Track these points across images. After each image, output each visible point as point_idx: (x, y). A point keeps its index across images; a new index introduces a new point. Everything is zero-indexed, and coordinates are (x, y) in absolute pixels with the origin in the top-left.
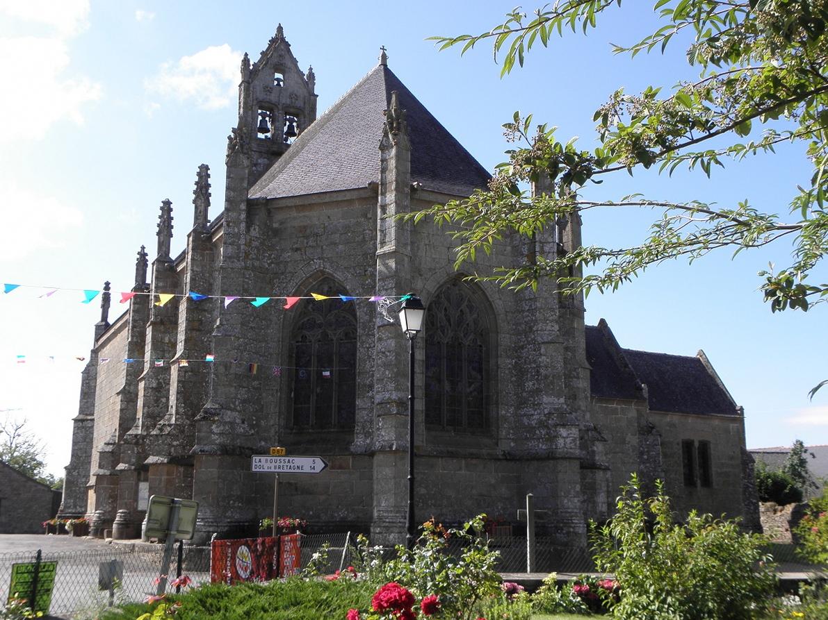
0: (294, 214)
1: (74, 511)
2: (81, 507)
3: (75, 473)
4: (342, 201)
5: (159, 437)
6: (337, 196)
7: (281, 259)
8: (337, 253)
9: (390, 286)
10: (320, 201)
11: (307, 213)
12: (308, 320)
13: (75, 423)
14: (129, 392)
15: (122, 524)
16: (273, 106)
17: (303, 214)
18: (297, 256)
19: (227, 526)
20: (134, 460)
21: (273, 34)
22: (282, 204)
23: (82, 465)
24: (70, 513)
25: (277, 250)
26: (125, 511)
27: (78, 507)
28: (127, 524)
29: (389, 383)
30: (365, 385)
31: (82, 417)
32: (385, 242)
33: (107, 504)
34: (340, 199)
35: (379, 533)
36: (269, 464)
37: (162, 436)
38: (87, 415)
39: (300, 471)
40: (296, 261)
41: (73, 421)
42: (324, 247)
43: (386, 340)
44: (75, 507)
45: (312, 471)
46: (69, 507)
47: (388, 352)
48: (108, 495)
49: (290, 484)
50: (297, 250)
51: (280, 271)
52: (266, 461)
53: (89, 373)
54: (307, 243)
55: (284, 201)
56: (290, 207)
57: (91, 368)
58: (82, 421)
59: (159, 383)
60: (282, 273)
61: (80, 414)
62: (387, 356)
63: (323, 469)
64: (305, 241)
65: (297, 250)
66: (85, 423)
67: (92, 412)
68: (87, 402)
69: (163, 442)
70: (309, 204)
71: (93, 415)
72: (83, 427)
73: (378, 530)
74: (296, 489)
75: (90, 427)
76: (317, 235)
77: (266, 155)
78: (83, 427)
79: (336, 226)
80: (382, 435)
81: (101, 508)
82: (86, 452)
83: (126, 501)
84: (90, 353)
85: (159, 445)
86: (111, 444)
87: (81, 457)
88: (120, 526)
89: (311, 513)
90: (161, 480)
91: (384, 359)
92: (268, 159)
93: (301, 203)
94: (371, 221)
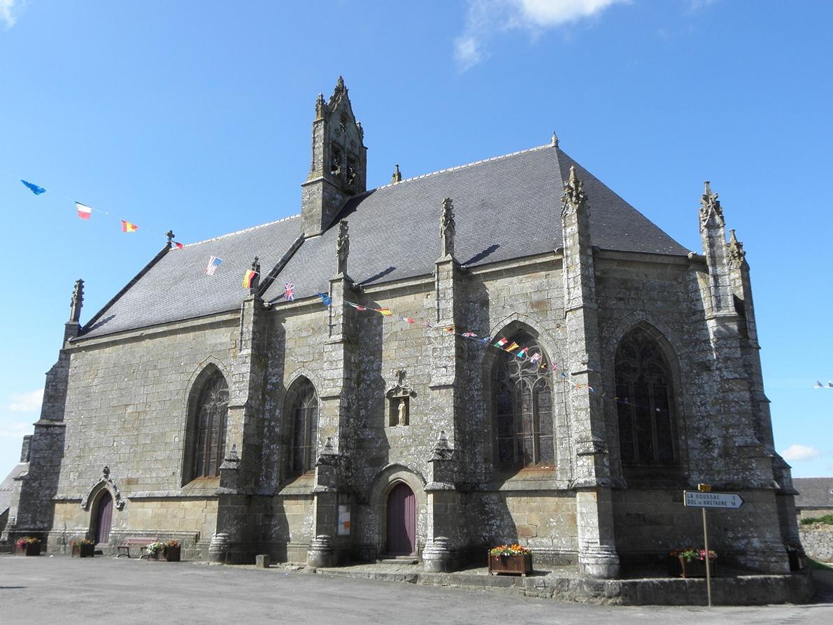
0: (615, 266)
1: (32, 527)
2: (42, 522)
3: (35, 484)
4: (659, 264)
5: (441, 462)
6: (663, 260)
7: (607, 306)
8: (657, 308)
9: (734, 345)
10: (642, 260)
11: (626, 268)
12: (623, 363)
13: (36, 428)
14: (251, 406)
15: (327, 551)
16: (340, 148)
17: (623, 268)
18: (621, 305)
19: (439, 554)
20: (333, 482)
21: (337, 84)
22: (607, 255)
23: (46, 476)
24: (26, 529)
25: (603, 297)
26: (326, 536)
27: (38, 523)
28: (332, 550)
29: (746, 429)
30: (694, 428)
31: (45, 422)
32: (720, 307)
33: (231, 526)
34: (659, 261)
35: (776, 562)
36: (699, 500)
37: (443, 461)
38: (52, 420)
39: (724, 506)
40: (620, 309)
41: (34, 426)
42: (645, 301)
43: (739, 392)
44: (34, 522)
45: (734, 507)
46: (26, 523)
47: (743, 402)
48: (233, 517)
49: (638, 515)
50: (621, 299)
51: (607, 317)
52: (697, 496)
53: (55, 374)
54: (629, 295)
55: (610, 253)
56: (613, 260)
57: (60, 370)
58: (47, 427)
59: (349, 403)
60: (610, 319)
61: (41, 418)
62: (741, 406)
63: (742, 505)
64: (628, 293)
65: (621, 299)
66: (51, 430)
67: (61, 418)
68: (54, 406)
69: (446, 468)
70: (632, 261)
71: (62, 420)
72: (48, 434)
73: (773, 559)
74: (645, 519)
75: (58, 435)
76: (637, 289)
77: (340, 192)
78: (48, 434)
79: (652, 284)
80: (757, 475)
81: (225, 530)
82: (51, 461)
83: (325, 525)
84: (59, 353)
85: (441, 471)
86: (234, 461)
87: (44, 466)
88: (326, 553)
89: (660, 542)
90: (447, 506)
91: (738, 407)
92: (342, 196)
93: (625, 259)
94: (682, 285)
